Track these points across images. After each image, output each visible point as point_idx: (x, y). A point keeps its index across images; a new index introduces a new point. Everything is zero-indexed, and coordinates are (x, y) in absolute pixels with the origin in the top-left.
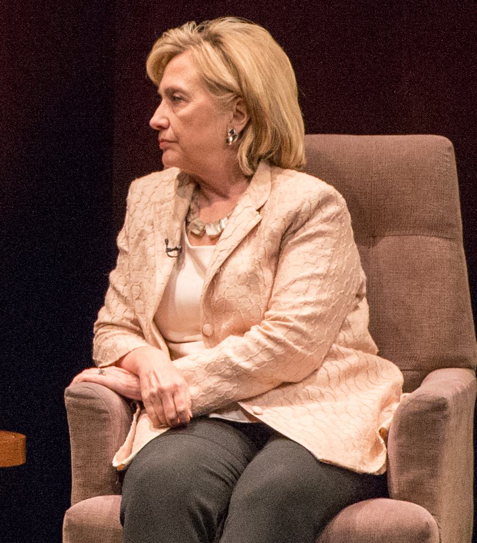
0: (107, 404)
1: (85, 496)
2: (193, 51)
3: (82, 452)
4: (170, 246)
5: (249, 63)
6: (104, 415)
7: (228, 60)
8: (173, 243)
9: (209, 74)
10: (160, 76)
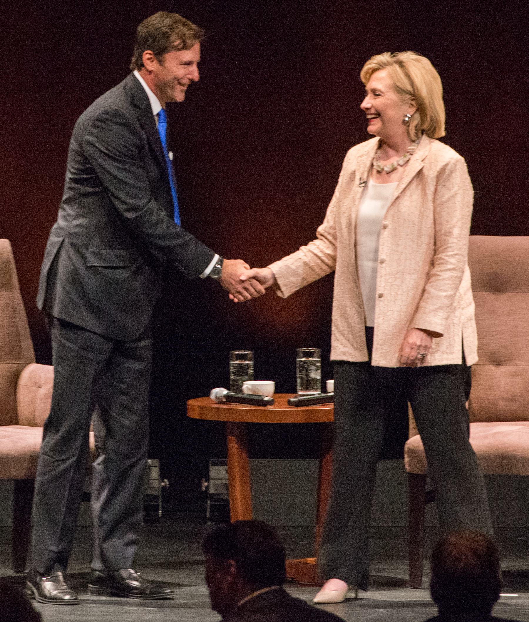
2: (389, 69)
10: (369, 80)
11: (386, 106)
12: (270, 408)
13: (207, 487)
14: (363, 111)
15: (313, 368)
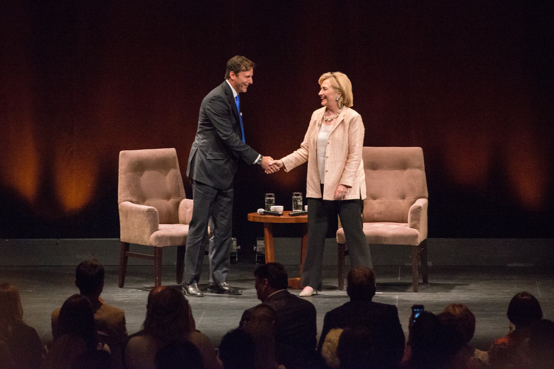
2: (330, 79)
7: (338, 82)
11: (329, 94)
12: (281, 217)
13: (256, 249)
15: (299, 200)
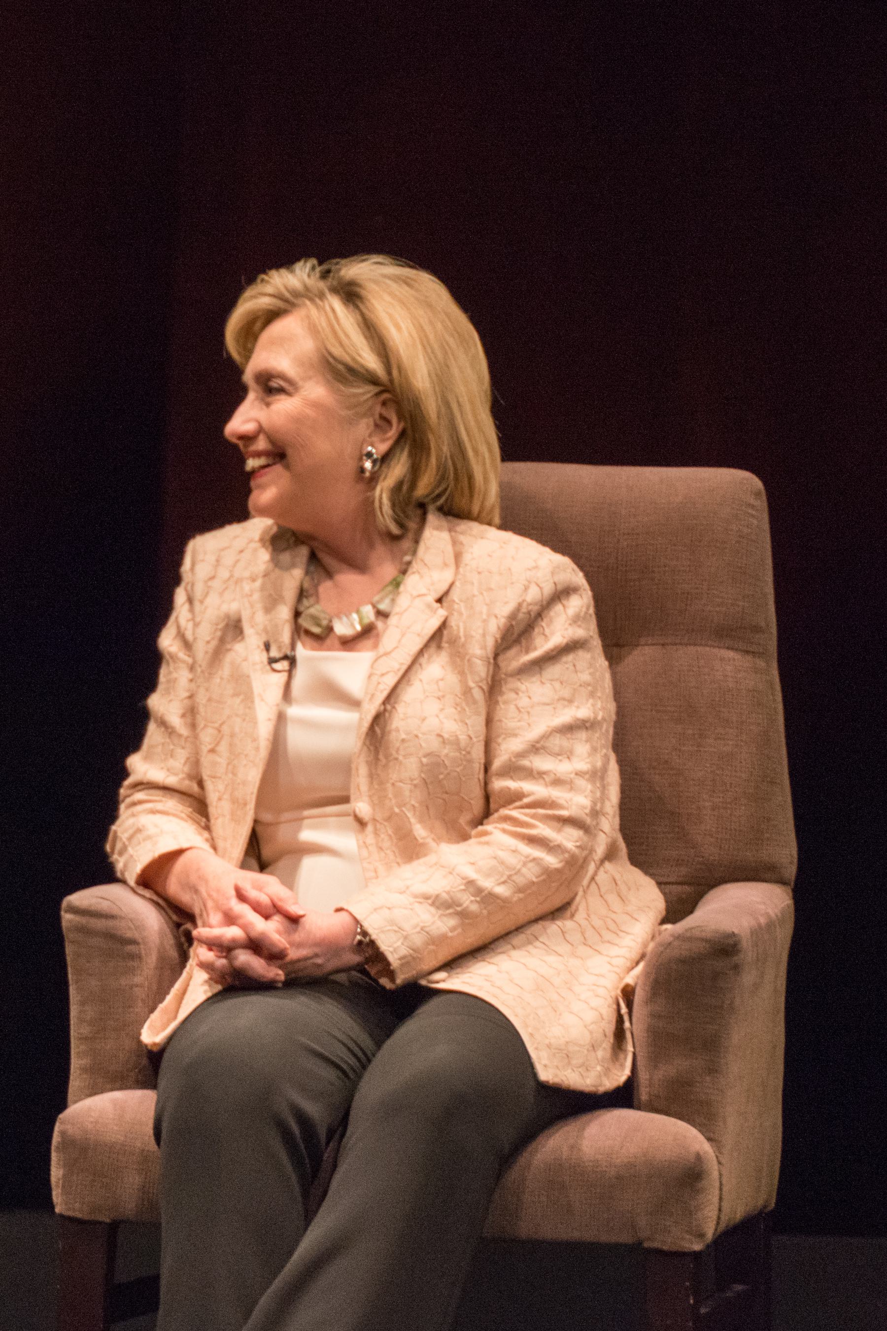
0: (137, 928)
1: (94, 1091)
2: (310, 309)
3: (90, 1012)
4: (274, 653)
5: (406, 334)
6: (131, 948)
7: (371, 329)
8: (280, 648)
9: (337, 351)
10: (248, 353)
11: (298, 420)
14: (235, 447)
